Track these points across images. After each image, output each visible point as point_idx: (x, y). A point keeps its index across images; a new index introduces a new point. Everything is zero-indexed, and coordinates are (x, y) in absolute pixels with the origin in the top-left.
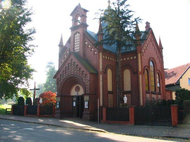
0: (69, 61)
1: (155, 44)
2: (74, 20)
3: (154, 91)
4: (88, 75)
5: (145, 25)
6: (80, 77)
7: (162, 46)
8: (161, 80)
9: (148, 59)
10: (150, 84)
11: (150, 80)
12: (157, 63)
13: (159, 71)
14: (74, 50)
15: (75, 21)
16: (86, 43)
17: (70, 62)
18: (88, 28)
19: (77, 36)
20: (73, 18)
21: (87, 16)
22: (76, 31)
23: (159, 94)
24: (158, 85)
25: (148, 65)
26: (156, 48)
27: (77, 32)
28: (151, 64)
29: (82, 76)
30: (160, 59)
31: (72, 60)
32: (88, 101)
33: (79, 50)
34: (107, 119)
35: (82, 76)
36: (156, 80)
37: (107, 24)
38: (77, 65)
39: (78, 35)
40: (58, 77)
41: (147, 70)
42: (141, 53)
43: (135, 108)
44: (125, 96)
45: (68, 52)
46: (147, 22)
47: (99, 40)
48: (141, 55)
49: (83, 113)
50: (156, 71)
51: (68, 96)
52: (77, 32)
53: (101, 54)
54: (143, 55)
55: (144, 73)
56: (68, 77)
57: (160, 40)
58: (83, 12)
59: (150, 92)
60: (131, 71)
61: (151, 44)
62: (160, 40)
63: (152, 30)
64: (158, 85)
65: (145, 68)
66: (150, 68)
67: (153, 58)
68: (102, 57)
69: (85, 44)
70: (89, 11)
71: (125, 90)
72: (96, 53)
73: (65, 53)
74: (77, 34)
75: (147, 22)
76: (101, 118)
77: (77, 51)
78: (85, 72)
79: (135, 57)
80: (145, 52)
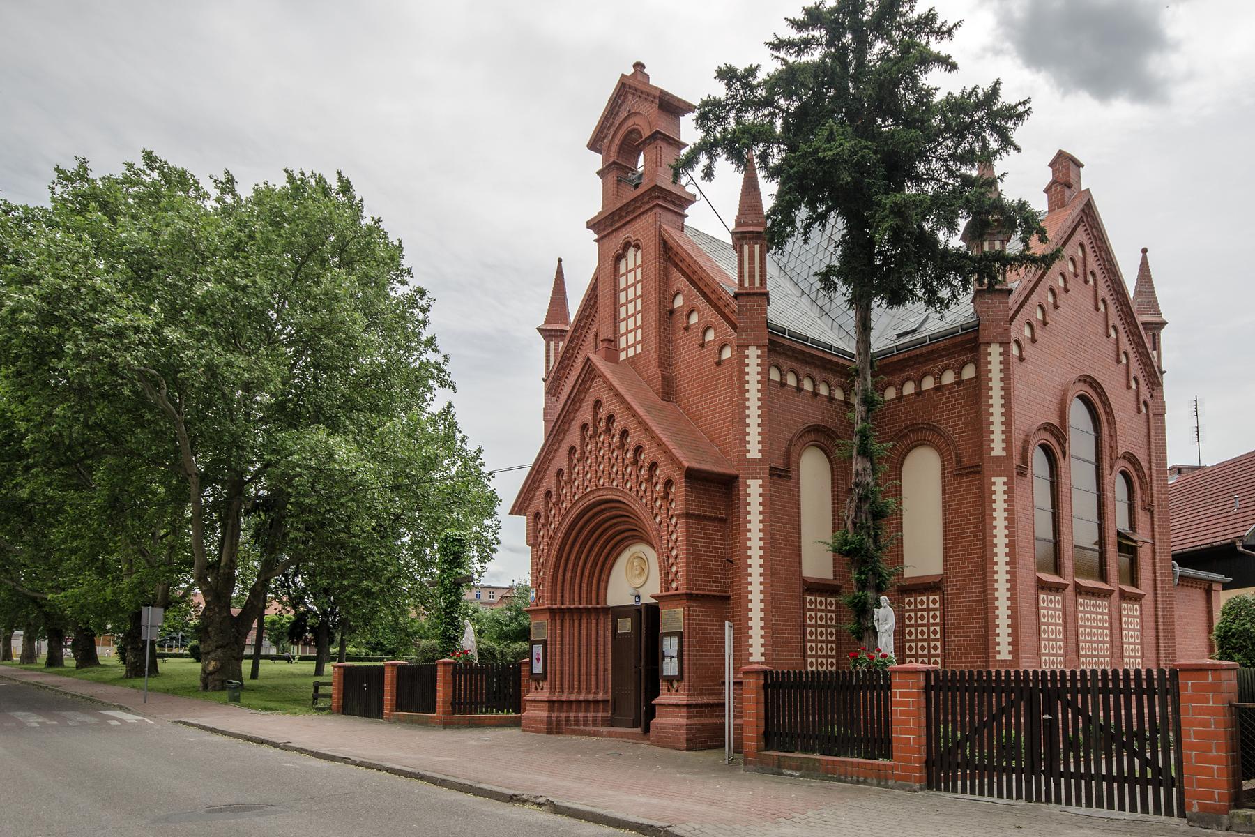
0: (585, 415)
1: (1120, 327)
13: (1130, 457)
16: (679, 302)
17: (589, 418)
19: (631, 266)
23: (1124, 596)
25: (1055, 421)
26: (1115, 319)
27: (627, 246)
28: (1078, 416)
29: (648, 493)
30: (1128, 365)
31: (598, 404)
40: (532, 510)
41: (1046, 449)
42: (1005, 344)
46: (1061, 154)
47: (1010, 492)
48: (1006, 353)
49: (655, 701)
50: (1113, 461)
52: (627, 246)
55: (1023, 470)
56: (575, 511)
57: (1144, 265)
60: (943, 462)
61: (1080, 296)
62: (1144, 265)
68: (764, 374)
69: (672, 312)
71: (908, 573)
72: (727, 354)
74: (631, 251)
75: (1061, 154)
79: (969, 372)
80: (1034, 341)
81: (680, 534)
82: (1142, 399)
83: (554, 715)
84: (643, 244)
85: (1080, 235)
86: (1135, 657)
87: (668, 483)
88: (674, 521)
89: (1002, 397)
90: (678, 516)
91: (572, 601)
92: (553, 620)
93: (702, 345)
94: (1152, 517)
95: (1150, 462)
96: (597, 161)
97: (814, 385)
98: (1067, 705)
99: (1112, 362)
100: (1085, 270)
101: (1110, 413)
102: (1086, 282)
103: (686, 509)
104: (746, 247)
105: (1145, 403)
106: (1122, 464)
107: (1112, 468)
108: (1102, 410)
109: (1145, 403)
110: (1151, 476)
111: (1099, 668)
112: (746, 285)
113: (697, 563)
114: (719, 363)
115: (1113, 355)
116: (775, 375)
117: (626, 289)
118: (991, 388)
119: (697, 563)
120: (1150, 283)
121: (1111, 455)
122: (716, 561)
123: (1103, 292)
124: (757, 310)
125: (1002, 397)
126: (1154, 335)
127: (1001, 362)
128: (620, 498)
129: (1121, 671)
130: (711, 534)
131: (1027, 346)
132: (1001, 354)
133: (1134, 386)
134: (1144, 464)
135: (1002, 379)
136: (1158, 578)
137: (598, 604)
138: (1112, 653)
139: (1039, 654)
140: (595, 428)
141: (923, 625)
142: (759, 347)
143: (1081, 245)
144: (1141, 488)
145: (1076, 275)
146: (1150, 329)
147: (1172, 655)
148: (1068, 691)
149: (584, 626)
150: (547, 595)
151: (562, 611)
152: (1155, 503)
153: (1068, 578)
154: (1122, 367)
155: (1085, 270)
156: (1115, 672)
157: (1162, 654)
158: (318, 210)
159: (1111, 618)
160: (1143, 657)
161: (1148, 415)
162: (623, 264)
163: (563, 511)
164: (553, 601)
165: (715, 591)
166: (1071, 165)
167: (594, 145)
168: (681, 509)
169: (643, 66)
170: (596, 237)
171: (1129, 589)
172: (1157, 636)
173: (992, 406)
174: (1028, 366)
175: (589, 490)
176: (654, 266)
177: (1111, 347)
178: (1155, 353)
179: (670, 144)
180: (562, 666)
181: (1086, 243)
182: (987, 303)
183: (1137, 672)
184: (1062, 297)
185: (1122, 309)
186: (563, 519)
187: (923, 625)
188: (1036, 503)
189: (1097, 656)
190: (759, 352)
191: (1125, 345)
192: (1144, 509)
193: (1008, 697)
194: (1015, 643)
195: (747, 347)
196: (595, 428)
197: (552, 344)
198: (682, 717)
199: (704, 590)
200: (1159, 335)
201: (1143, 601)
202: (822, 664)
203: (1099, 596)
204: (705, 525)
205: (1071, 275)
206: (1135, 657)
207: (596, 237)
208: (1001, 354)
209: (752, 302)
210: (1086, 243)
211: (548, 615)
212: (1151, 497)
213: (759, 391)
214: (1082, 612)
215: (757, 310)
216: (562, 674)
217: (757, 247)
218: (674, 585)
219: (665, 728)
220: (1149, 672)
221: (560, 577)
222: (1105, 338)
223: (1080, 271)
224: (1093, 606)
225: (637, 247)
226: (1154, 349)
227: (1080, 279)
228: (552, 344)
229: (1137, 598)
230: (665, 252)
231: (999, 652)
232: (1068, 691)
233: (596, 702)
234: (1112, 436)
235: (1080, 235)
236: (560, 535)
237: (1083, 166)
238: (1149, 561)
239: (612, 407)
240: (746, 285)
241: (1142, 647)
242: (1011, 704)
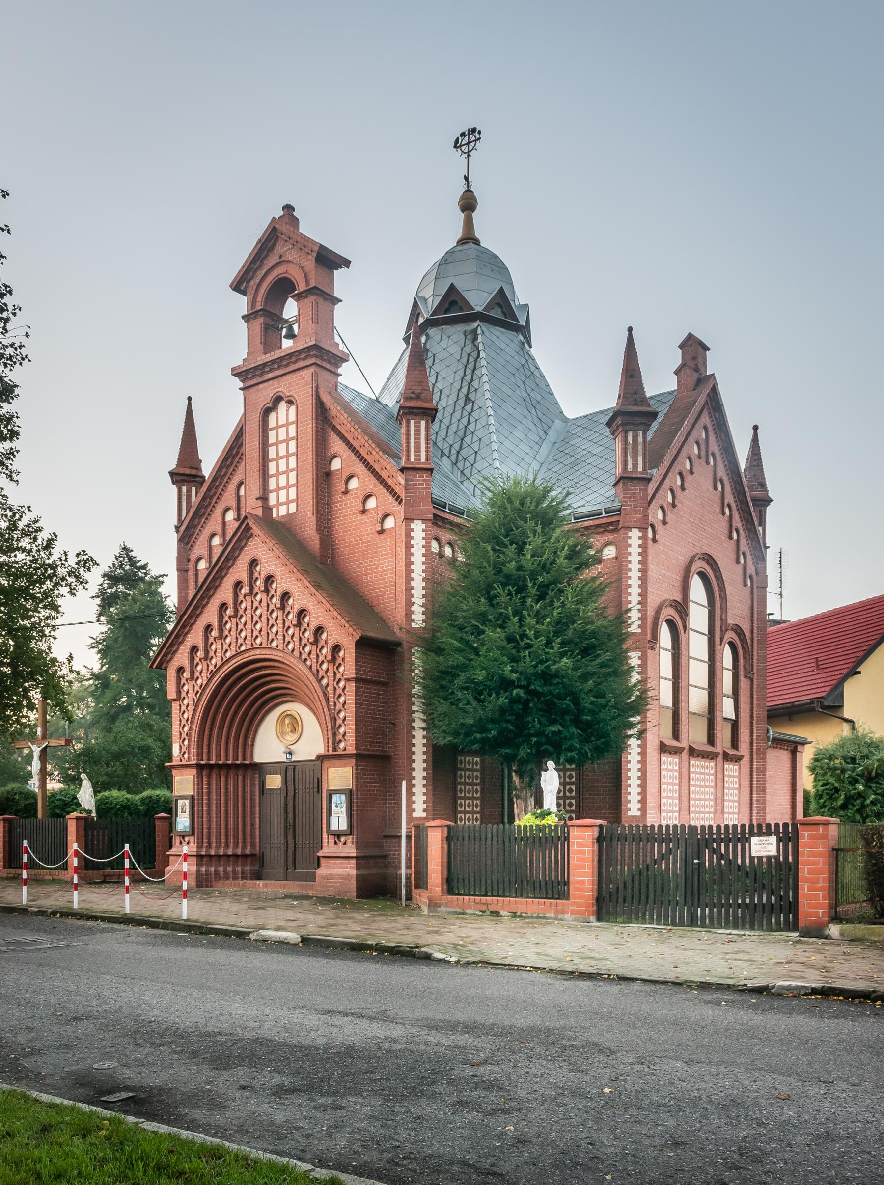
0: (239, 571)
1: (733, 505)
2: (259, 322)
3: (704, 739)
4: (349, 654)
5: (676, 359)
6: (320, 681)
7: (763, 485)
8: (744, 683)
9: (682, 559)
10: (683, 705)
11: (683, 683)
12: (729, 589)
13: (738, 630)
14: (267, 509)
15: (267, 328)
16: (336, 465)
18: (345, 369)
19: (282, 421)
20: (253, 303)
21: (337, 294)
22: (267, 392)
23: (727, 757)
24: (727, 708)
26: (729, 498)
28: (697, 591)
29: (313, 656)
30: (738, 541)
31: (254, 563)
32: (350, 794)
33: (293, 508)
34: (451, 885)
35: (313, 656)
36: (717, 679)
37: (625, 667)
38: (319, 630)
39: (284, 414)
41: (671, 623)
43: (601, 831)
44: (551, 764)
45: (230, 516)
46: (690, 336)
48: (644, 538)
49: (320, 854)
51: (246, 767)
52: (278, 399)
53: (418, 527)
54: (654, 540)
55: (655, 637)
56: (227, 669)
57: (755, 440)
58: (310, 263)
59: (684, 744)
62: (755, 440)
63: (714, 390)
64: (727, 708)
65: (662, 616)
66: (687, 614)
67: (709, 560)
68: (427, 547)
70: (347, 263)
72: (389, 523)
73: (214, 524)
74: (283, 405)
75: (690, 336)
76: (420, 881)
77: (283, 511)
78: (332, 636)
80: (664, 522)
81: (350, 697)
82: (748, 573)
83: (203, 869)
84: (298, 398)
85: (705, 419)
86: (733, 813)
87: (336, 648)
88: (342, 684)
89: (640, 578)
90: (348, 680)
91: (219, 757)
92: (200, 776)
93: (364, 511)
94: (752, 685)
95: (753, 636)
96: (241, 304)
97: (453, 551)
98: (714, 851)
99: (724, 538)
100: (707, 451)
101: (722, 587)
102: (708, 463)
103: (356, 674)
104: (412, 422)
105: (751, 577)
106: (730, 635)
107: (722, 640)
108: (716, 585)
109: (751, 577)
110: (752, 646)
111: (707, 824)
112: (413, 459)
113: (364, 725)
114: (382, 531)
115: (726, 532)
116: (435, 545)
117: (277, 444)
118: (630, 570)
119: (364, 725)
120: (759, 459)
121: (721, 627)
122: (379, 723)
123: (722, 472)
124: (422, 485)
125: (640, 578)
126: (760, 511)
127: (640, 546)
128: (280, 659)
129: (723, 826)
130: (375, 698)
131: (660, 528)
132: (640, 538)
133: (742, 561)
134: (748, 634)
135: (640, 562)
136: (755, 741)
137: (244, 760)
138: (715, 809)
139: (660, 811)
140: (251, 588)
141: (569, 784)
142: (424, 521)
143: (705, 428)
144: (744, 657)
145: (699, 457)
146: (758, 505)
147: (763, 812)
148: (714, 841)
149: (231, 781)
150: (193, 751)
151: (210, 767)
152: (755, 671)
153: (718, 749)
154: (733, 543)
155: (707, 451)
156: (719, 827)
157: (755, 810)
158: (622, 661)
159: (716, 778)
160: (739, 813)
161: (752, 588)
162: (272, 418)
163: (211, 668)
164: (200, 756)
165: (377, 750)
166: (700, 348)
167: (238, 286)
168: (350, 674)
169: (293, 209)
170: (241, 385)
171: (732, 752)
172: (751, 794)
173: (630, 586)
174: (659, 547)
175: (243, 648)
176: (309, 427)
177: (725, 525)
178: (760, 528)
179: (325, 299)
180: (209, 821)
181: (709, 426)
182: (630, 490)
183: (735, 826)
184: (688, 478)
185: (735, 488)
186: (212, 676)
187: (569, 784)
188: (661, 675)
189: (704, 812)
190: (424, 526)
191: (737, 522)
192: (746, 677)
193: (667, 846)
194: (643, 801)
195: (413, 520)
196: (251, 588)
197: (184, 489)
198: (351, 868)
199: (369, 750)
200: (765, 512)
201: (742, 762)
202: (469, 819)
203: (707, 758)
204: (370, 689)
205: (696, 457)
206: (733, 813)
207: (241, 385)
208: (640, 538)
209: (420, 478)
210: (709, 426)
211: (194, 771)
212: (752, 665)
213: (423, 563)
214: (694, 773)
215: (422, 485)
216: (209, 828)
217: (423, 423)
218: (342, 745)
219: (334, 878)
220: (743, 826)
221: (207, 733)
222: (721, 516)
223: (703, 453)
224: (703, 767)
225: (290, 402)
226: (760, 525)
227: (703, 461)
228: (184, 489)
229: (737, 759)
230: (322, 413)
231: (629, 809)
232: (714, 841)
233: (245, 856)
234: (724, 609)
235: (705, 419)
236: (209, 691)
237: (708, 349)
238: (748, 724)
239: (272, 568)
240: (413, 459)
241: (739, 804)
242: (670, 851)
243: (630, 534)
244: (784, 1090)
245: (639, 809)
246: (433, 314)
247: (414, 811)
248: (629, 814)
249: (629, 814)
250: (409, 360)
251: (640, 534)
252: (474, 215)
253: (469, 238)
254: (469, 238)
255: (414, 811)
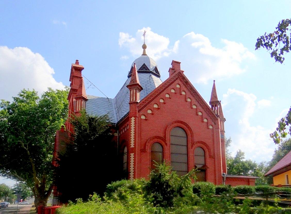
46: (173, 61)
75: (173, 61)
243: (131, 119)
244: (22, 94)
245: (134, 146)
246: (139, 70)
247: (134, 155)
248: (131, 147)
249: (131, 147)
250: (160, 34)
251: (134, 118)
252: (146, 50)
253: (144, 54)
254: (144, 54)
255: (134, 155)
